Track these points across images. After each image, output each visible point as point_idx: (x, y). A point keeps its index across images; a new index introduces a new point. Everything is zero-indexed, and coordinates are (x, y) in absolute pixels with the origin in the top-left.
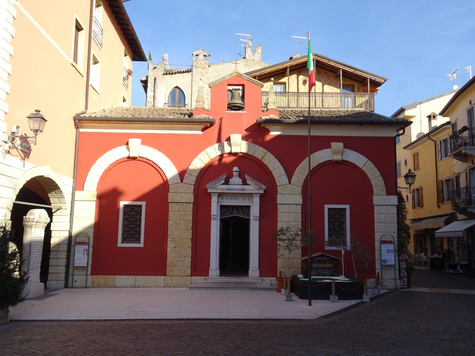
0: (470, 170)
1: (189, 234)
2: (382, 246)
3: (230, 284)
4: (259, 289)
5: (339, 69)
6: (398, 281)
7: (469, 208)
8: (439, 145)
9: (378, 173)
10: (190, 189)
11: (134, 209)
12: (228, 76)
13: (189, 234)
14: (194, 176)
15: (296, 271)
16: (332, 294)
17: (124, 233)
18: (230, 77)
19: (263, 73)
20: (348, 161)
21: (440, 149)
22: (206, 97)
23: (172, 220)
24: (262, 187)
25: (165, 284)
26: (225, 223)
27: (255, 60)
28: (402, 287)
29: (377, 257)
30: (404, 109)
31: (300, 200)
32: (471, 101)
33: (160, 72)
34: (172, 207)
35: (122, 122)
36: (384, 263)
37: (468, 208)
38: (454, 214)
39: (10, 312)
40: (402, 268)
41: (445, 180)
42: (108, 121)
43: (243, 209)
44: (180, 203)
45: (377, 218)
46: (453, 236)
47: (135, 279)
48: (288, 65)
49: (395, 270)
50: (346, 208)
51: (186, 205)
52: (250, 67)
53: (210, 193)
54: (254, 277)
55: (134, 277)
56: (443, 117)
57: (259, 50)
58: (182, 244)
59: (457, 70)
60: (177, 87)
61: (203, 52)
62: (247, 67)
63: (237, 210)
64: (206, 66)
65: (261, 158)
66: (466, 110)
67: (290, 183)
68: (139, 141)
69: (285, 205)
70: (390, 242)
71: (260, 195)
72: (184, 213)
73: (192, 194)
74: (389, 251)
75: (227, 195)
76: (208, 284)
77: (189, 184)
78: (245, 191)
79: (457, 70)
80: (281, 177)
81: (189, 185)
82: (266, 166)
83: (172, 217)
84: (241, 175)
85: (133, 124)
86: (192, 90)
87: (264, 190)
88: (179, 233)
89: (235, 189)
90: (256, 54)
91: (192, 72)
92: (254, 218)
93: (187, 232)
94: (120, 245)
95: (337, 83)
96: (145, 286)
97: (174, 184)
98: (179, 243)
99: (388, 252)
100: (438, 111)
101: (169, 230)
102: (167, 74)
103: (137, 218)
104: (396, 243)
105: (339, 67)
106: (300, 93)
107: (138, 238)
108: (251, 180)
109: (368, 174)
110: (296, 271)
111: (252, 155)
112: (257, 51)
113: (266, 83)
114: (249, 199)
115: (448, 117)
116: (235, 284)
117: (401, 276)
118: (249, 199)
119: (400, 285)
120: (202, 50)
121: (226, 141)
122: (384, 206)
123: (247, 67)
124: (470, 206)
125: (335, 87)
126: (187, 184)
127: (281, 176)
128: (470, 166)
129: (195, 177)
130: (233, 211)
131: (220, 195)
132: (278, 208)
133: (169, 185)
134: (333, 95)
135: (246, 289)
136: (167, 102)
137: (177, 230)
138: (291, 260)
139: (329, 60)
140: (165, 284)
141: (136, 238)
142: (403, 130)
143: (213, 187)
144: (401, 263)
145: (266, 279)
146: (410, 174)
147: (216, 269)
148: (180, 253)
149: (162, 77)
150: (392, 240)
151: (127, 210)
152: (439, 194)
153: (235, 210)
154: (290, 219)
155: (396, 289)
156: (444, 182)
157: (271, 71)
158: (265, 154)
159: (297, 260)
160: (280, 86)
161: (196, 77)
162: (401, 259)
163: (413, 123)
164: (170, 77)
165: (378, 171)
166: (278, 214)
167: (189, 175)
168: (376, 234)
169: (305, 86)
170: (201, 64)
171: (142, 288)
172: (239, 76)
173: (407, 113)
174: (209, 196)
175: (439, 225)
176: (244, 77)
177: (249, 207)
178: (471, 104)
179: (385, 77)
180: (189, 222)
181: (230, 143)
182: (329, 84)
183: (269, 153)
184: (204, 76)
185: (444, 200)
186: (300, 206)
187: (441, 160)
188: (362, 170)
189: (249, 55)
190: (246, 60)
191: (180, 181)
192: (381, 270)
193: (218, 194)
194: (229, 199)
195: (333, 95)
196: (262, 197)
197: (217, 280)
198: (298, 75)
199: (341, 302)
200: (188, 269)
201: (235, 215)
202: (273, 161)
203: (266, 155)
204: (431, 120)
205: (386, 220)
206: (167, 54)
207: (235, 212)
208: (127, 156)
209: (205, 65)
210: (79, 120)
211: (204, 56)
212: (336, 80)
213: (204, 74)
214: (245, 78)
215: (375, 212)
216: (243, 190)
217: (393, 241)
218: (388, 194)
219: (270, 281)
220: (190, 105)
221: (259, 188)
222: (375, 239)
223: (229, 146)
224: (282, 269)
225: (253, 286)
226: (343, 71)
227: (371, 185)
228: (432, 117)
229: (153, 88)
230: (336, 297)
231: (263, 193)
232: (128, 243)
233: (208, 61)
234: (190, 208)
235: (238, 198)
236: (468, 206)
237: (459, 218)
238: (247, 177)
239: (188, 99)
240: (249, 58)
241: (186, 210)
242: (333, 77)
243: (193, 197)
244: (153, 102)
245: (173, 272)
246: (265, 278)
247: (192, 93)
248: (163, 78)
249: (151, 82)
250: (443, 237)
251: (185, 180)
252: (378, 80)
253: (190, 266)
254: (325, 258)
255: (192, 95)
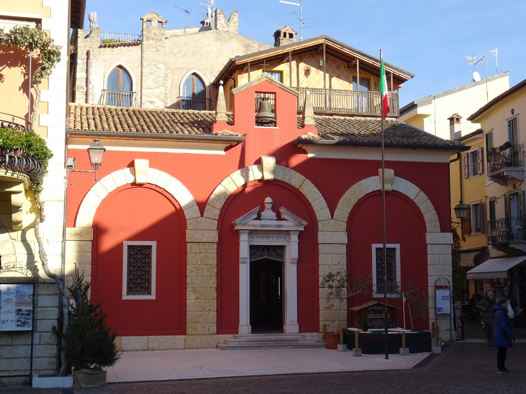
0: (511, 197)
1: (214, 282)
2: (437, 292)
3: (267, 342)
4: (305, 347)
5: (354, 58)
6: (453, 332)
7: (512, 243)
8: (466, 159)
9: (431, 206)
10: (213, 225)
11: (140, 251)
12: (256, 82)
13: (213, 282)
14: (217, 209)
15: (342, 324)
16: (402, 347)
17: (129, 281)
18: (258, 82)
19: (257, 59)
20: (398, 192)
21: (466, 164)
22: (163, 82)
23: (192, 265)
24: (302, 223)
25: (185, 346)
26: (254, 268)
27: (229, 31)
28: (457, 339)
29: (431, 304)
30: (416, 105)
31: (344, 238)
32: (513, 110)
33: (95, 43)
34: (191, 248)
35: (125, 138)
36: (439, 312)
37: (510, 243)
38: (486, 250)
39: (107, 373)
40: (457, 317)
41: (472, 205)
42: (109, 137)
43: (275, 249)
44: (201, 243)
45: (430, 259)
46: (492, 278)
47: (148, 340)
48: (290, 50)
49: (450, 319)
50: (396, 248)
51: (209, 246)
52: (223, 42)
53: (237, 230)
54: (293, 333)
55: (146, 337)
56: (473, 123)
57: (236, 19)
58: (205, 295)
59: (484, 57)
60: (120, 67)
61: (157, 17)
62: (219, 42)
63: (269, 251)
64: (162, 37)
65: (299, 187)
66: (506, 120)
67: (332, 218)
68: (146, 162)
69: (327, 245)
70: (445, 287)
71: (299, 232)
72: (207, 256)
73: (216, 231)
74: (444, 297)
75: (258, 232)
76: (242, 343)
77: (211, 219)
78: (282, 228)
79: (484, 57)
80: (323, 210)
81: (211, 220)
82: (304, 196)
83: (191, 260)
84: (275, 208)
85: (140, 140)
86: (142, 72)
87: (304, 226)
88: (201, 280)
89: (270, 226)
90: (231, 24)
91: (142, 45)
92: (292, 260)
93: (211, 279)
94: (125, 297)
95: (348, 75)
96: (160, 348)
97: (193, 218)
98: (201, 294)
99: (443, 299)
100: (466, 113)
101: (188, 278)
102: (105, 46)
103: (145, 263)
104: (451, 288)
105: (355, 56)
106: (301, 88)
107: (148, 288)
108: (289, 214)
109: (420, 207)
110: (342, 324)
111: (288, 182)
112: (232, 20)
113: (255, 70)
114: (285, 237)
115: (479, 123)
116: (274, 342)
117: (457, 326)
118: (285, 237)
119: (455, 336)
120: (156, 14)
121: (255, 164)
122: (438, 245)
123: (219, 42)
124: (512, 241)
125: (347, 81)
126: (209, 218)
127: (322, 209)
128: (511, 191)
129: (219, 209)
130: (263, 252)
131: (252, 233)
132: (319, 248)
133: (186, 220)
134: (348, 93)
135: (290, 347)
136: (105, 88)
137: (198, 278)
138: (335, 311)
139: (343, 46)
140: (185, 346)
141: (145, 288)
142: (457, 154)
143: (244, 223)
144: (456, 312)
145: (307, 334)
146: (461, 206)
147: (247, 325)
148: (203, 306)
149: (98, 51)
150: (447, 284)
151: (132, 252)
152: (465, 223)
153: (266, 250)
154: (334, 261)
155: (451, 341)
156: (471, 207)
157: (268, 56)
158: (304, 182)
159: (342, 311)
160: (274, 75)
161: (148, 53)
162: (456, 307)
163: (471, 148)
164: (109, 50)
165: (432, 204)
166: (320, 255)
167: (212, 207)
168: (429, 277)
169: (307, 77)
170: (155, 34)
171: (157, 351)
172: (270, 81)
173: (420, 110)
174: (237, 233)
175: (467, 263)
176: (275, 84)
177: (283, 248)
178: (513, 113)
179: (412, 73)
180: (213, 267)
181: (261, 166)
182: (339, 77)
183: (308, 180)
184: (160, 52)
185: (472, 230)
186: (344, 246)
187: (468, 178)
188: (413, 202)
189: (222, 24)
190: (217, 31)
191: (200, 216)
192: (436, 319)
193: (248, 231)
194: (260, 237)
195: (348, 93)
196: (301, 235)
197: (250, 337)
198: (299, 61)
199: (412, 355)
200: (214, 325)
201: (266, 257)
202: (313, 190)
203: (305, 182)
204: (453, 123)
205: (440, 262)
206: (96, 12)
207: (266, 254)
208: (132, 182)
209: (160, 35)
210: (70, 134)
211: (159, 22)
212: (348, 71)
213: (160, 49)
214: (277, 85)
215: (429, 252)
216: (280, 226)
217: (449, 286)
218: (442, 231)
219: (312, 337)
220: (140, 94)
221: (298, 224)
222: (428, 284)
223: (259, 170)
224: (326, 322)
225: (295, 343)
226: (361, 62)
227: (424, 220)
228: (455, 120)
229: (85, 67)
230: (408, 350)
231: (303, 230)
232: (135, 294)
233: (165, 30)
234: (214, 249)
235: (271, 236)
236: (510, 241)
237: (491, 255)
238: (282, 210)
239: (136, 85)
240: (222, 29)
241: (209, 251)
242: (344, 67)
243: (218, 235)
244: (85, 88)
245: (195, 329)
246: (305, 334)
247: (142, 76)
248: (99, 52)
249: (83, 58)
250: (494, 278)
251: (207, 213)
252: (403, 76)
253: (216, 322)
254: (381, 307)
255: (142, 79)
